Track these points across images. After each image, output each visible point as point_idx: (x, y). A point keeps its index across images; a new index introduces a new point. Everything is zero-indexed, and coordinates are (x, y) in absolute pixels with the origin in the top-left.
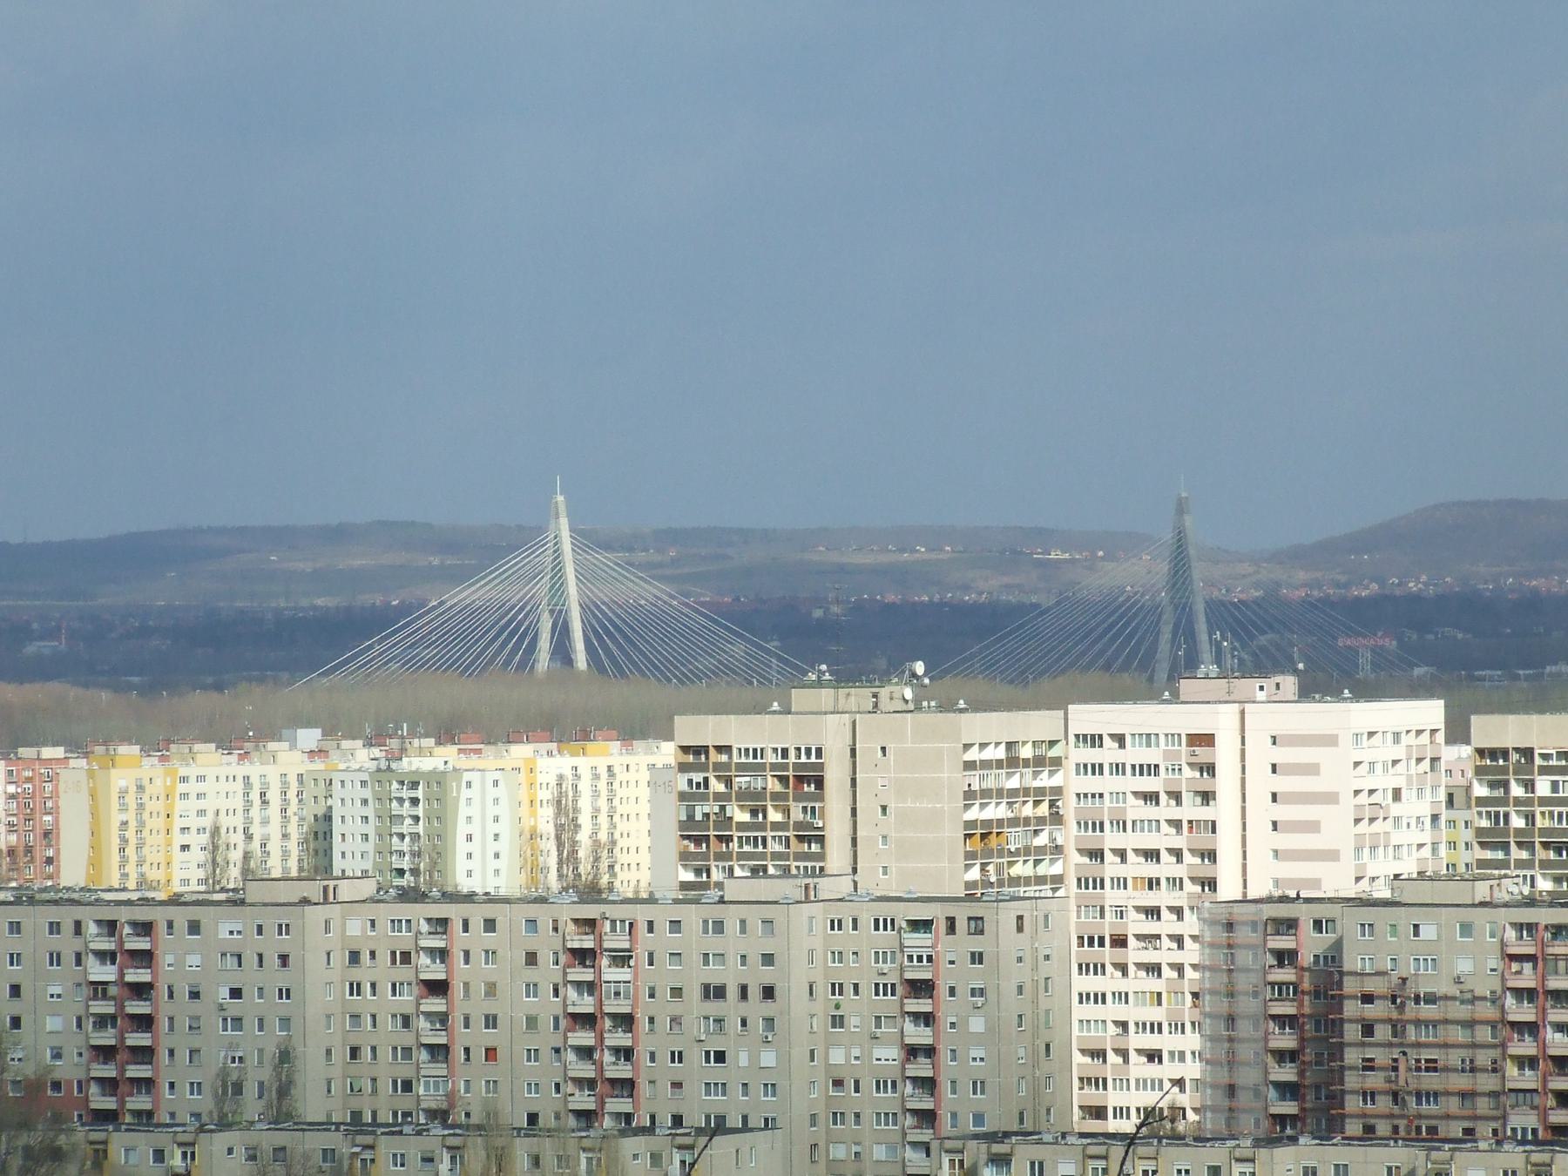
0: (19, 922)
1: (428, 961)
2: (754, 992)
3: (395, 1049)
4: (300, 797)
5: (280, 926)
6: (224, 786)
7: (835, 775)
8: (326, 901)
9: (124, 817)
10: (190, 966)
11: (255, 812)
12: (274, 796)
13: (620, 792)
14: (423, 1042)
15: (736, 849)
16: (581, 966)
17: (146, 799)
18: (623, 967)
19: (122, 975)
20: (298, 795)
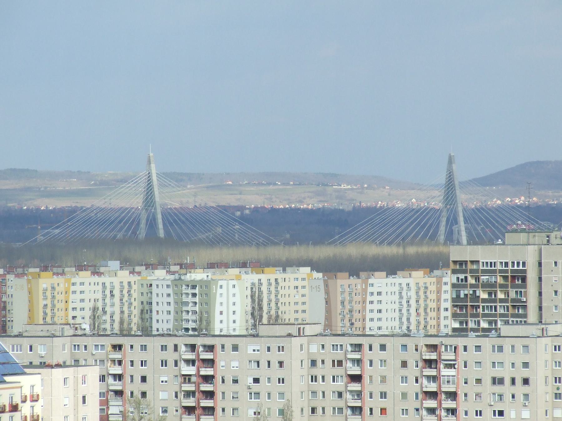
0: (146, 345)
1: (351, 365)
2: (519, 381)
3: (334, 408)
4: (129, 293)
5: (279, 347)
6: (93, 287)
7: (532, 276)
8: (299, 335)
9: (45, 302)
10: (233, 367)
11: (108, 300)
12: (117, 292)
13: (281, 292)
14: (349, 405)
15: (481, 312)
16: (429, 368)
17: (56, 294)
18: (451, 368)
19: (198, 371)
20: (128, 292)
